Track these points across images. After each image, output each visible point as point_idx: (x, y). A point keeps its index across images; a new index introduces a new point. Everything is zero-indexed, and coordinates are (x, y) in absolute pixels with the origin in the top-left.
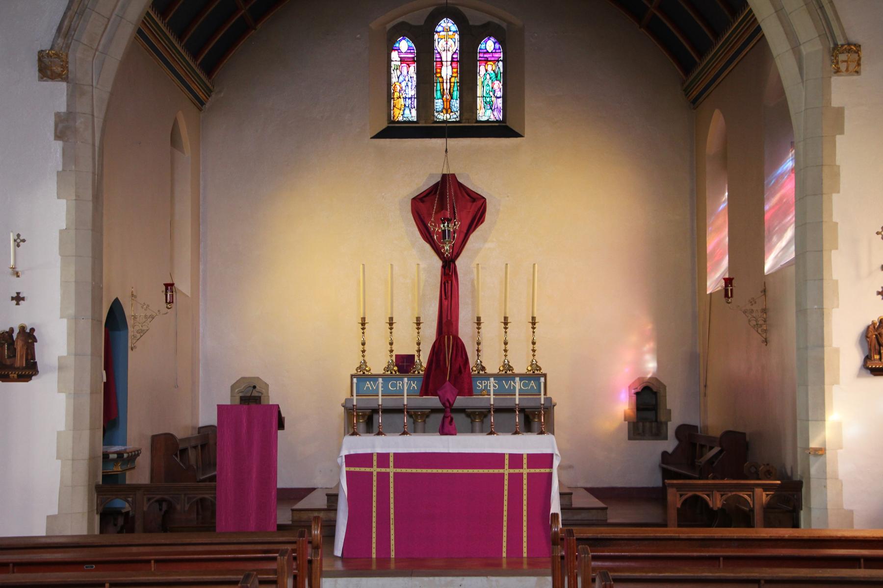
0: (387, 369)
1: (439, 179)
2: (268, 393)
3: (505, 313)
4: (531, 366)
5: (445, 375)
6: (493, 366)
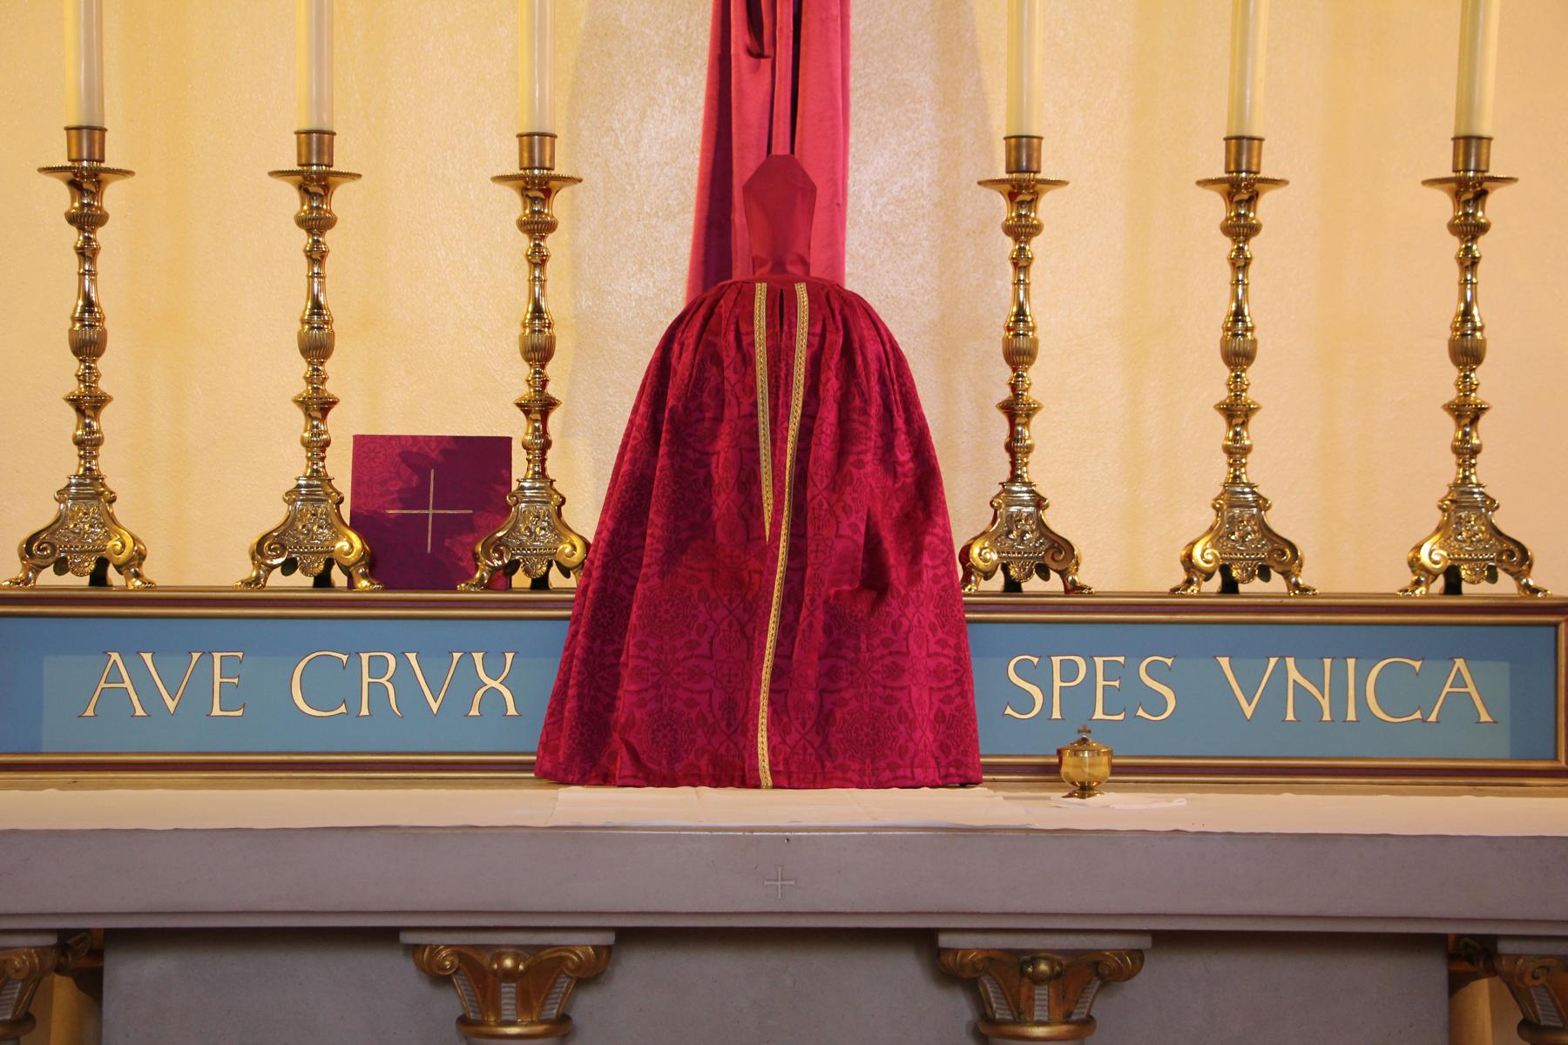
0: (276, 547)
3: (1239, 106)
4: (1217, 535)
6: (1131, 524)
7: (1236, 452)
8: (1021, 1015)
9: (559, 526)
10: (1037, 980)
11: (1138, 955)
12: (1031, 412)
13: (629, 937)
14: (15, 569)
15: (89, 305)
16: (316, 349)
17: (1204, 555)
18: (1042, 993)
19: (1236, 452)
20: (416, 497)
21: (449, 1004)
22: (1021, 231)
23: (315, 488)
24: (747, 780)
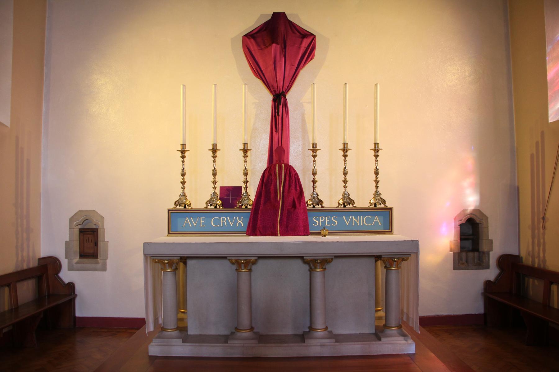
0: (209, 202)
1: (270, 18)
2: (103, 226)
3: (344, 139)
4: (343, 199)
5: (278, 199)
6: (331, 198)
7: (345, 187)
8: (316, 268)
9: (249, 199)
10: (318, 263)
11: (332, 259)
12: (316, 182)
13: (259, 258)
14: (174, 206)
15: (183, 169)
16: (214, 174)
17: (341, 202)
18: (319, 265)
19: (345, 187)
20: (228, 195)
21: (234, 267)
22: (314, 156)
23: (215, 194)
24: (276, 235)
